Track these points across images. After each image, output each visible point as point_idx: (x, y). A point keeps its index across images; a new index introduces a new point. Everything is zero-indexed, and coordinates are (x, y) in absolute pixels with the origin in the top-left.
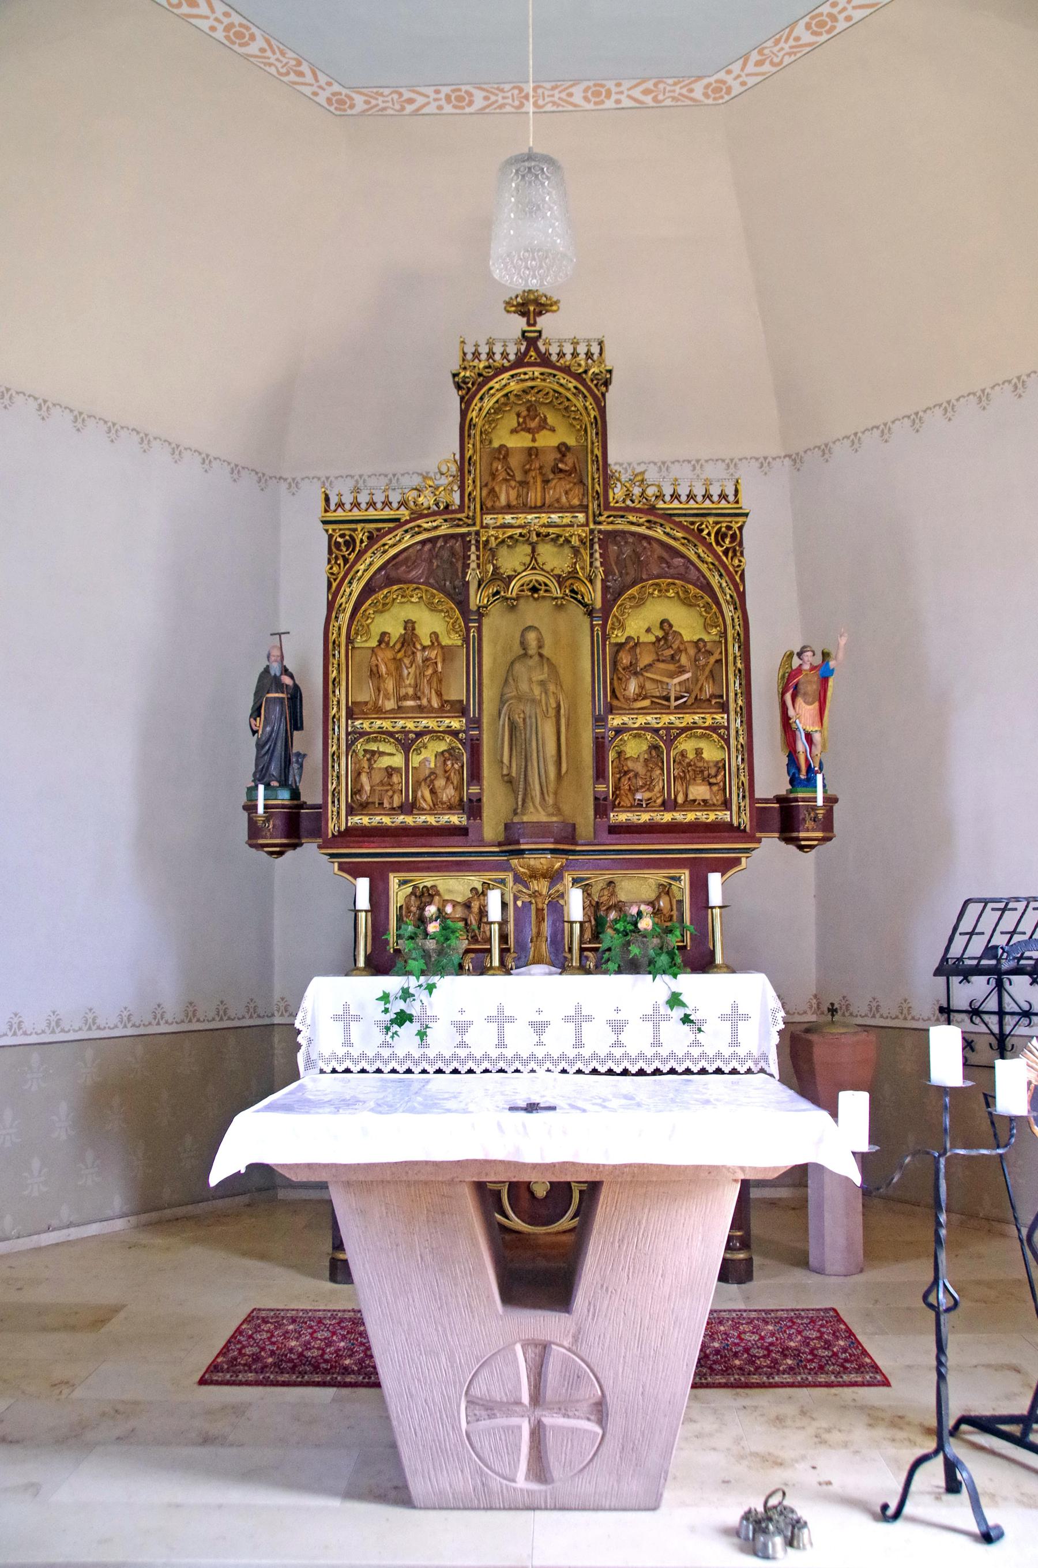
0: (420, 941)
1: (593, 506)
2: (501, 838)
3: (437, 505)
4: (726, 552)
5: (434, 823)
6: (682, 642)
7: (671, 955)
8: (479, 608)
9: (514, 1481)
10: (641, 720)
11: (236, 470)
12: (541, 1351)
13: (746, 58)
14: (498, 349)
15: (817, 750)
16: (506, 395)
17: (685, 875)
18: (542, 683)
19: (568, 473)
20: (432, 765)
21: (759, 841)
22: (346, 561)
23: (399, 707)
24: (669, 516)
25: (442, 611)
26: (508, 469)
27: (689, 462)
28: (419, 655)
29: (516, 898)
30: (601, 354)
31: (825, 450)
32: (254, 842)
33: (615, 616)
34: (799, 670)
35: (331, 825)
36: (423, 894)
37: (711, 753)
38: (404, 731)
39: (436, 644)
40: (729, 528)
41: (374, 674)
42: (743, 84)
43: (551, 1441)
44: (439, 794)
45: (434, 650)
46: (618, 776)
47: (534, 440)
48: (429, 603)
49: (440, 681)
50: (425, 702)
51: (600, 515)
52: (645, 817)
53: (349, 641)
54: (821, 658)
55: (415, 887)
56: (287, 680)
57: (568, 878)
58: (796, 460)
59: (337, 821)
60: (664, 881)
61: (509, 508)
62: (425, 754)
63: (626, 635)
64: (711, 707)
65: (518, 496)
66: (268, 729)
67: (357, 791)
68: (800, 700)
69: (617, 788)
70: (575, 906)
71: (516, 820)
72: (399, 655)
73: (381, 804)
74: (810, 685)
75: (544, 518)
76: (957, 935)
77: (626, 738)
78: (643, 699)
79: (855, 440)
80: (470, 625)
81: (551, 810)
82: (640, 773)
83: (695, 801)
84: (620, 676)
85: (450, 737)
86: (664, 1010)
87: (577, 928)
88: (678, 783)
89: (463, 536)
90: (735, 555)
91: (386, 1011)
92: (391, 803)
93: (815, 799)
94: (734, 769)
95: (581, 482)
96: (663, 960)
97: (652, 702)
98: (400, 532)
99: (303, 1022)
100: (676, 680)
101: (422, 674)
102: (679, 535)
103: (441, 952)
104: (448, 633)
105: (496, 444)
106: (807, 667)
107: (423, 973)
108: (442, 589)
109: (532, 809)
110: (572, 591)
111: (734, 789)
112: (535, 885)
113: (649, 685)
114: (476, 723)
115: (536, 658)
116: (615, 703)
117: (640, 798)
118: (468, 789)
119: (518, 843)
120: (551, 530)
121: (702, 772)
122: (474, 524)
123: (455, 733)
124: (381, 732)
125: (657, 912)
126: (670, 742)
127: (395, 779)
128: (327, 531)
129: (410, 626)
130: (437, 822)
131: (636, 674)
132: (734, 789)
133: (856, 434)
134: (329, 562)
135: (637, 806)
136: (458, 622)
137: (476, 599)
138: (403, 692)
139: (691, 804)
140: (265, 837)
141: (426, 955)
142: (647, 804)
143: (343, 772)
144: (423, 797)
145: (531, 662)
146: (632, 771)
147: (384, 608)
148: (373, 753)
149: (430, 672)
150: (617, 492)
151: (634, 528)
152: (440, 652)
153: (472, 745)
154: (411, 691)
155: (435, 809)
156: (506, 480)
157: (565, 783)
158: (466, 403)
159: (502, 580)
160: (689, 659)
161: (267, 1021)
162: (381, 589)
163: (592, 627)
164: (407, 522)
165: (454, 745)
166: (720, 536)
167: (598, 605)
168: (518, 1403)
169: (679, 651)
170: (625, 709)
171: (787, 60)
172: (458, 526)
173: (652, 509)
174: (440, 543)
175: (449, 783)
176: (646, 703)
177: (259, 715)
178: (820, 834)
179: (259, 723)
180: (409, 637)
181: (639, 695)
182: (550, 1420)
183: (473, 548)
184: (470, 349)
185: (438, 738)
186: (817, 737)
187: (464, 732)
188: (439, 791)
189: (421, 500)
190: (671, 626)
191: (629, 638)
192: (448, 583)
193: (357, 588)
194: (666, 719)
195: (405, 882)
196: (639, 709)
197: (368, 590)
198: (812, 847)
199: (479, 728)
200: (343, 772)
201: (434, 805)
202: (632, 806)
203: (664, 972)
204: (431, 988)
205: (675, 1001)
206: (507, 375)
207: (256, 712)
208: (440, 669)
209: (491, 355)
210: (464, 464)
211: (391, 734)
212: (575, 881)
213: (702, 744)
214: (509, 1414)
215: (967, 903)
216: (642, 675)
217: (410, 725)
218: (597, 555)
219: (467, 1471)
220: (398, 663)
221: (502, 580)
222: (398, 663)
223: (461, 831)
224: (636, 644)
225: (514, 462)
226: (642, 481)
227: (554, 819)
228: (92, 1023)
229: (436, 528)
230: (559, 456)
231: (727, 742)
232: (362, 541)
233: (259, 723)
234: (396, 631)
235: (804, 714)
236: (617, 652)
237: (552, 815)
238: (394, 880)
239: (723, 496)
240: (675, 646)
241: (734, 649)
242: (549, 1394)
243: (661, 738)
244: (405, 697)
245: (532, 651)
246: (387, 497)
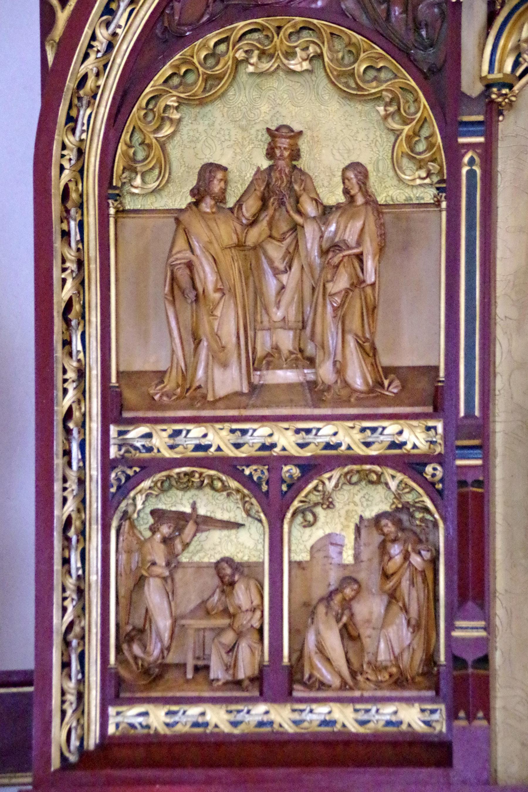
5: (353, 728)
8: (489, 86)
20: (348, 557)
23: (253, 388)
25: (378, 98)
39: (360, 200)
44: (366, 641)
45: (353, 217)
48: (341, 74)
80: (462, 140)
85: (400, 476)
104: (396, 165)
118: (449, 627)
130: (363, 723)
136: (425, 132)
144: (321, 650)
152: (372, 227)
153: (463, 499)
155: (356, 686)
165: (409, 498)
175: (395, 608)
185: (365, 477)
187: (440, 459)
188: (365, 632)
192: (397, 10)
201: (353, 674)
208: (370, 278)
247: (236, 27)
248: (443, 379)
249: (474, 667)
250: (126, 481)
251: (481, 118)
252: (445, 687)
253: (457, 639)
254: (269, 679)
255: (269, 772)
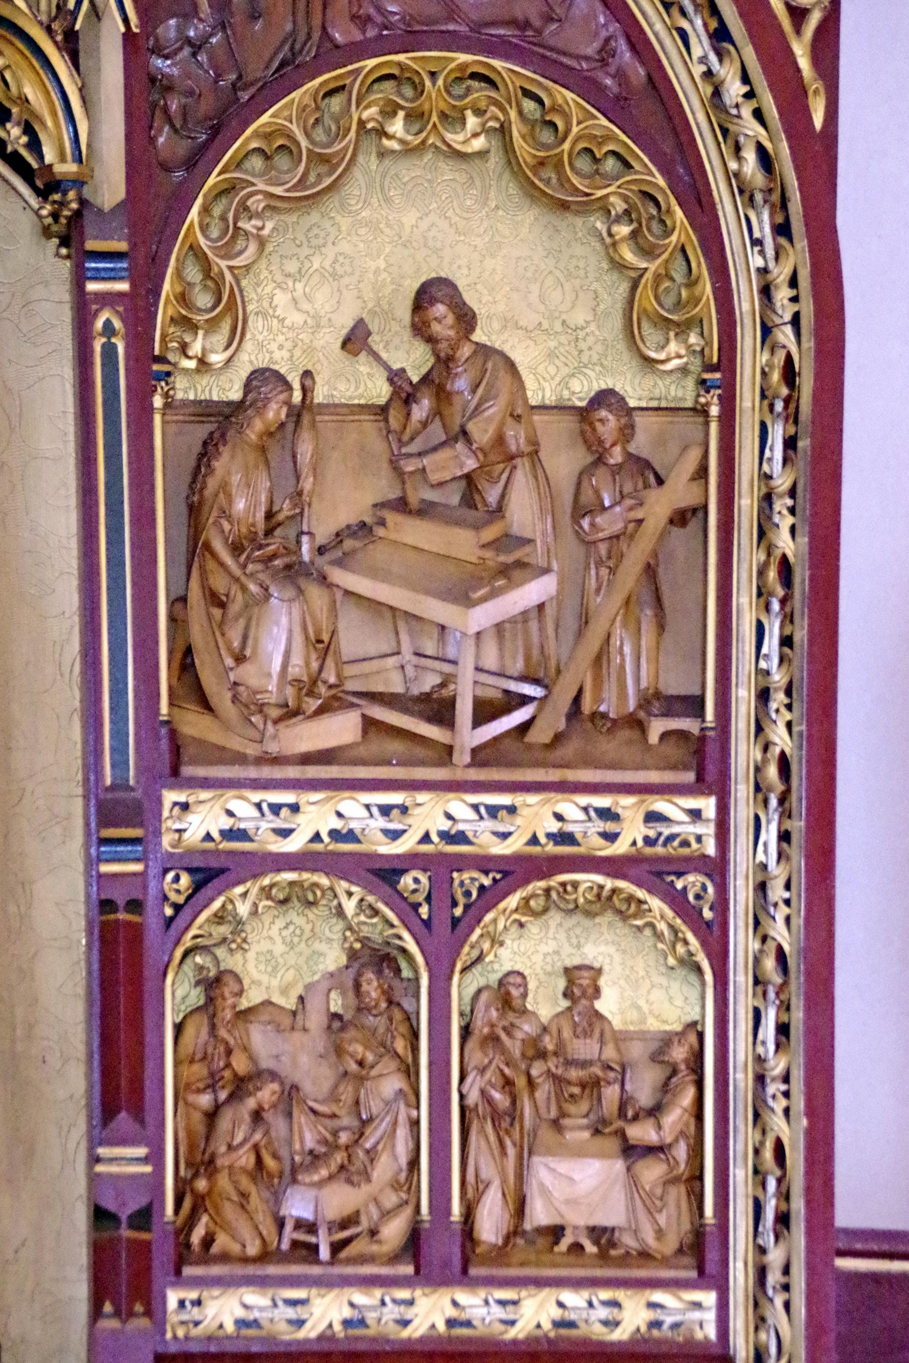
33: (194, 250)
46: (205, 1100)
77: (243, 909)
78: (321, 711)
82: (307, 1087)
84: (219, 583)
97: (370, 725)
117: (307, 1214)
142: (337, 1247)
146: (274, 1076)
170: (241, 759)
196: (306, 759)
202: (265, 1257)
216: (323, 579)
224: (297, 414)
247: (362, 68)
248: (713, 725)
249: (131, 1226)
250: (479, 896)
251: (123, 246)
253: (98, 1175)
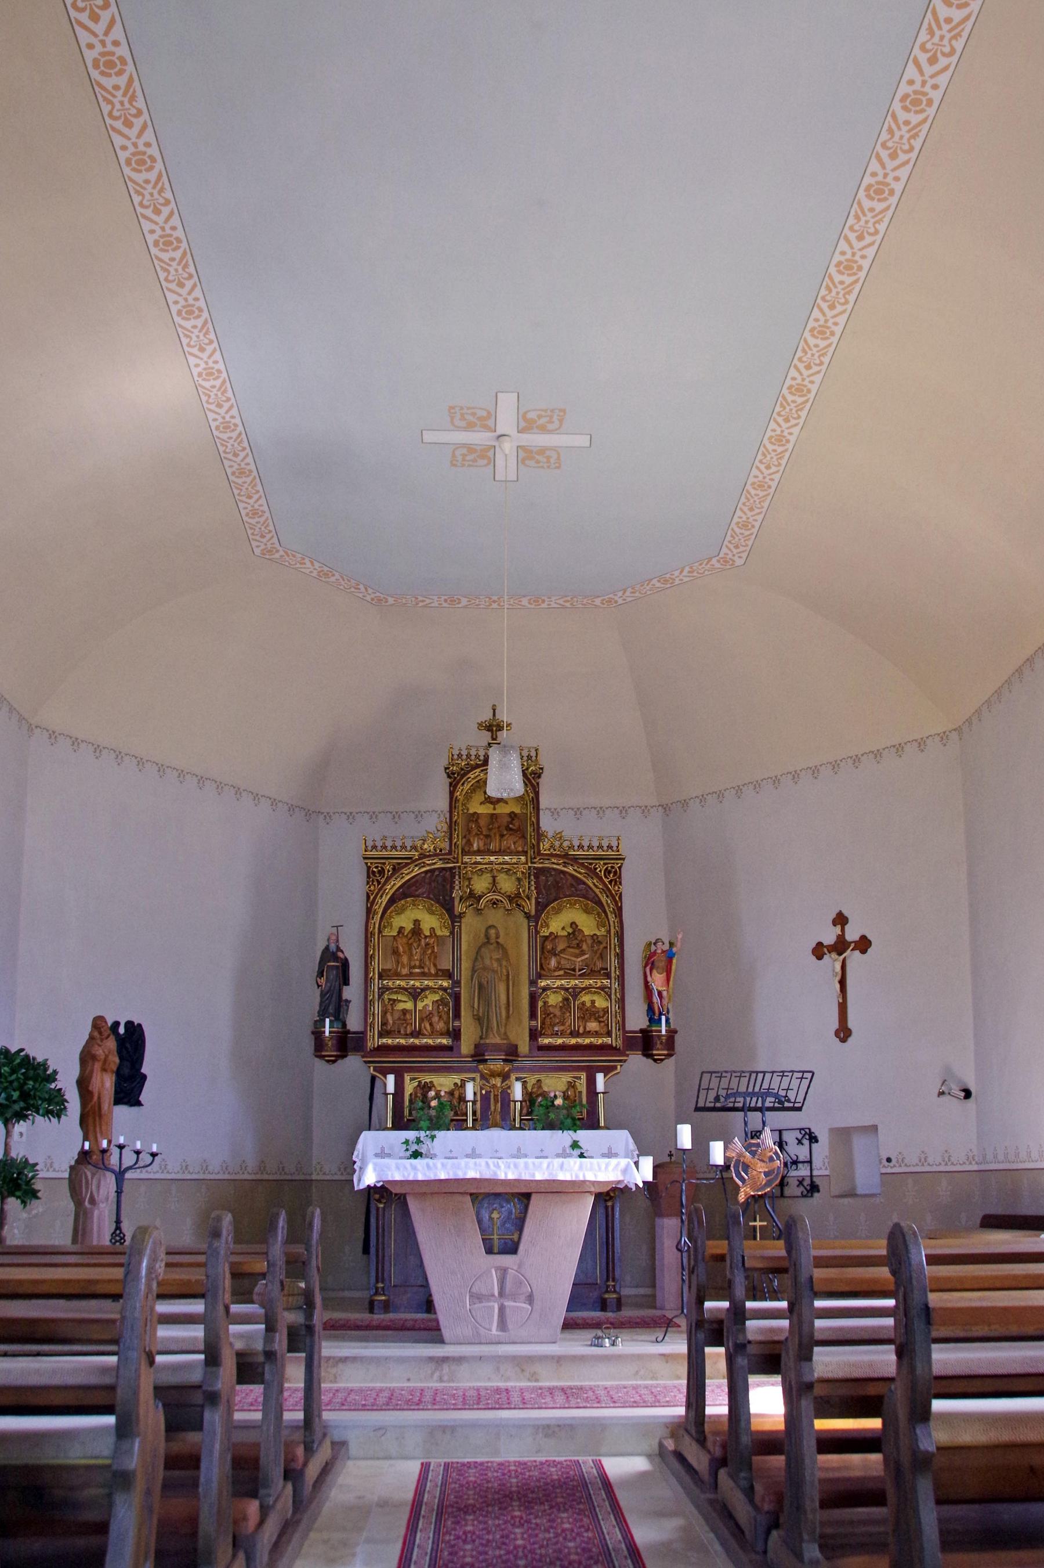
0: (426, 1111)
1: (530, 853)
2: (472, 1052)
3: (435, 850)
4: (610, 882)
6: (584, 936)
7: (574, 1119)
9: (490, 1330)
10: (558, 983)
11: (291, 809)
12: (503, 1272)
13: (625, 591)
14: (473, 752)
15: (665, 1002)
16: (478, 781)
17: (583, 1076)
18: (498, 960)
19: (516, 831)
20: (431, 1009)
21: (627, 1056)
22: (379, 883)
23: (411, 973)
24: (575, 860)
26: (479, 827)
27: (595, 808)
28: (423, 940)
29: (481, 1089)
30: (536, 757)
31: (685, 804)
32: (319, 1054)
34: (655, 953)
35: (369, 1044)
36: (424, 1086)
37: (601, 1003)
38: (413, 987)
40: (612, 867)
41: (395, 952)
42: (624, 600)
43: (508, 1311)
47: (494, 809)
49: (436, 957)
50: (426, 970)
51: (535, 858)
52: (560, 1041)
53: (380, 932)
54: (668, 945)
55: (420, 1082)
56: (340, 954)
57: (513, 1077)
58: (666, 808)
59: (374, 1040)
60: (570, 1080)
61: (479, 852)
62: (426, 1001)
63: (550, 931)
64: (601, 975)
65: (485, 845)
66: (329, 984)
67: (384, 1023)
68: (654, 972)
69: (543, 1023)
70: (517, 1092)
71: (482, 1042)
72: (410, 941)
73: (399, 1032)
74: (662, 964)
75: (501, 859)
76: (701, 1091)
79: (702, 799)
81: (503, 1037)
83: (589, 1032)
86: (569, 1150)
87: (518, 1105)
88: (580, 1020)
89: (451, 869)
90: (616, 884)
91: (407, 1150)
92: (406, 1031)
93: (660, 1031)
94: (614, 1013)
95: (524, 837)
96: (569, 1121)
98: (412, 866)
99: (357, 1156)
100: (579, 959)
101: (424, 953)
102: (583, 871)
103: (438, 1117)
104: (441, 928)
105: (471, 811)
106: (659, 951)
107: (429, 1129)
108: (438, 901)
109: (491, 1036)
110: (517, 905)
111: (614, 1024)
112: (493, 1081)
113: (563, 962)
114: (457, 983)
115: (495, 945)
116: (543, 972)
119: (484, 1055)
120: (504, 866)
121: (595, 1014)
122: (457, 862)
123: (445, 989)
124: (400, 987)
125: (566, 1097)
126: (575, 996)
127: (408, 1016)
128: (366, 864)
129: (417, 922)
131: (555, 955)
132: (614, 1024)
133: (703, 796)
134: (368, 883)
135: (556, 1034)
137: (459, 908)
138: (413, 964)
139: (587, 1034)
140: (327, 1051)
141: (430, 1119)
143: (376, 1012)
144: (425, 1028)
145: (492, 947)
147: (401, 911)
148: (394, 1000)
149: (430, 951)
150: (544, 846)
151: (555, 866)
154: (417, 963)
156: (477, 834)
157: (511, 1020)
158: (453, 787)
159: (475, 898)
160: (588, 946)
161: (308, 1178)
162: (400, 900)
163: (529, 926)
164: (417, 860)
166: (607, 872)
167: (533, 913)
168: (493, 1295)
169: (582, 941)
171: (649, 593)
172: (448, 863)
173: (566, 856)
174: (437, 873)
176: (561, 973)
177: (323, 976)
178: (665, 1052)
179: (323, 981)
180: (417, 931)
181: (557, 968)
182: (508, 1303)
183: (457, 877)
184: (456, 752)
186: (665, 994)
187: (451, 989)
189: (426, 846)
190: (577, 926)
191: (551, 933)
193: (385, 899)
194: (574, 982)
195: (414, 1079)
197: (392, 901)
198: (662, 1060)
199: (460, 987)
200: (376, 1012)
203: (569, 1129)
204: (433, 1137)
205: (575, 1145)
206: (478, 770)
207: (320, 974)
209: (469, 756)
210: (452, 825)
211: (406, 989)
212: (517, 1079)
213: (595, 997)
214: (489, 1301)
215: (703, 1073)
217: (418, 984)
218: (533, 883)
219: (470, 1327)
220: (410, 946)
221: (475, 898)
222: (410, 946)
223: (449, 1049)
225: (482, 822)
226: (561, 837)
227: (505, 1042)
228: (205, 1169)
229: (434, 864)
230: (510, 820)
231: (610, 996)
232: (389, 871)
233: (323, 981)
234: (409, 926)
235: (657, 981)
236: (544, 941)
237: (504, 1039)
238: (407, 1078)
239: (610, 847)
240: (579, 938)
241: (615, 941)
242: (507, 1291)
243: (570, 994)
244: (414, 967)
245: (493, 941)
246: (404, 843)
252: (452, 1035)
254: (415, 1034)
255: (605, 1531)
